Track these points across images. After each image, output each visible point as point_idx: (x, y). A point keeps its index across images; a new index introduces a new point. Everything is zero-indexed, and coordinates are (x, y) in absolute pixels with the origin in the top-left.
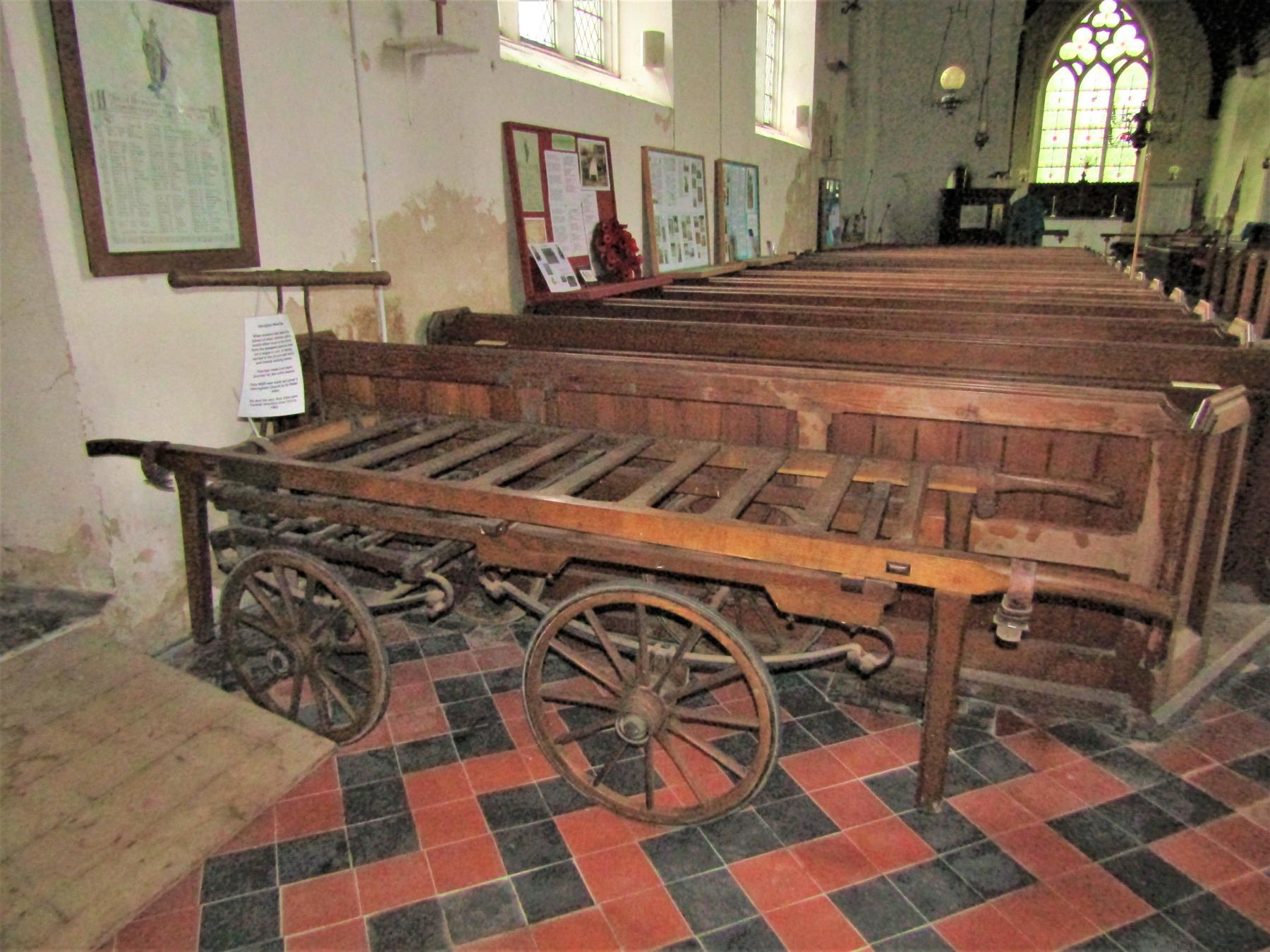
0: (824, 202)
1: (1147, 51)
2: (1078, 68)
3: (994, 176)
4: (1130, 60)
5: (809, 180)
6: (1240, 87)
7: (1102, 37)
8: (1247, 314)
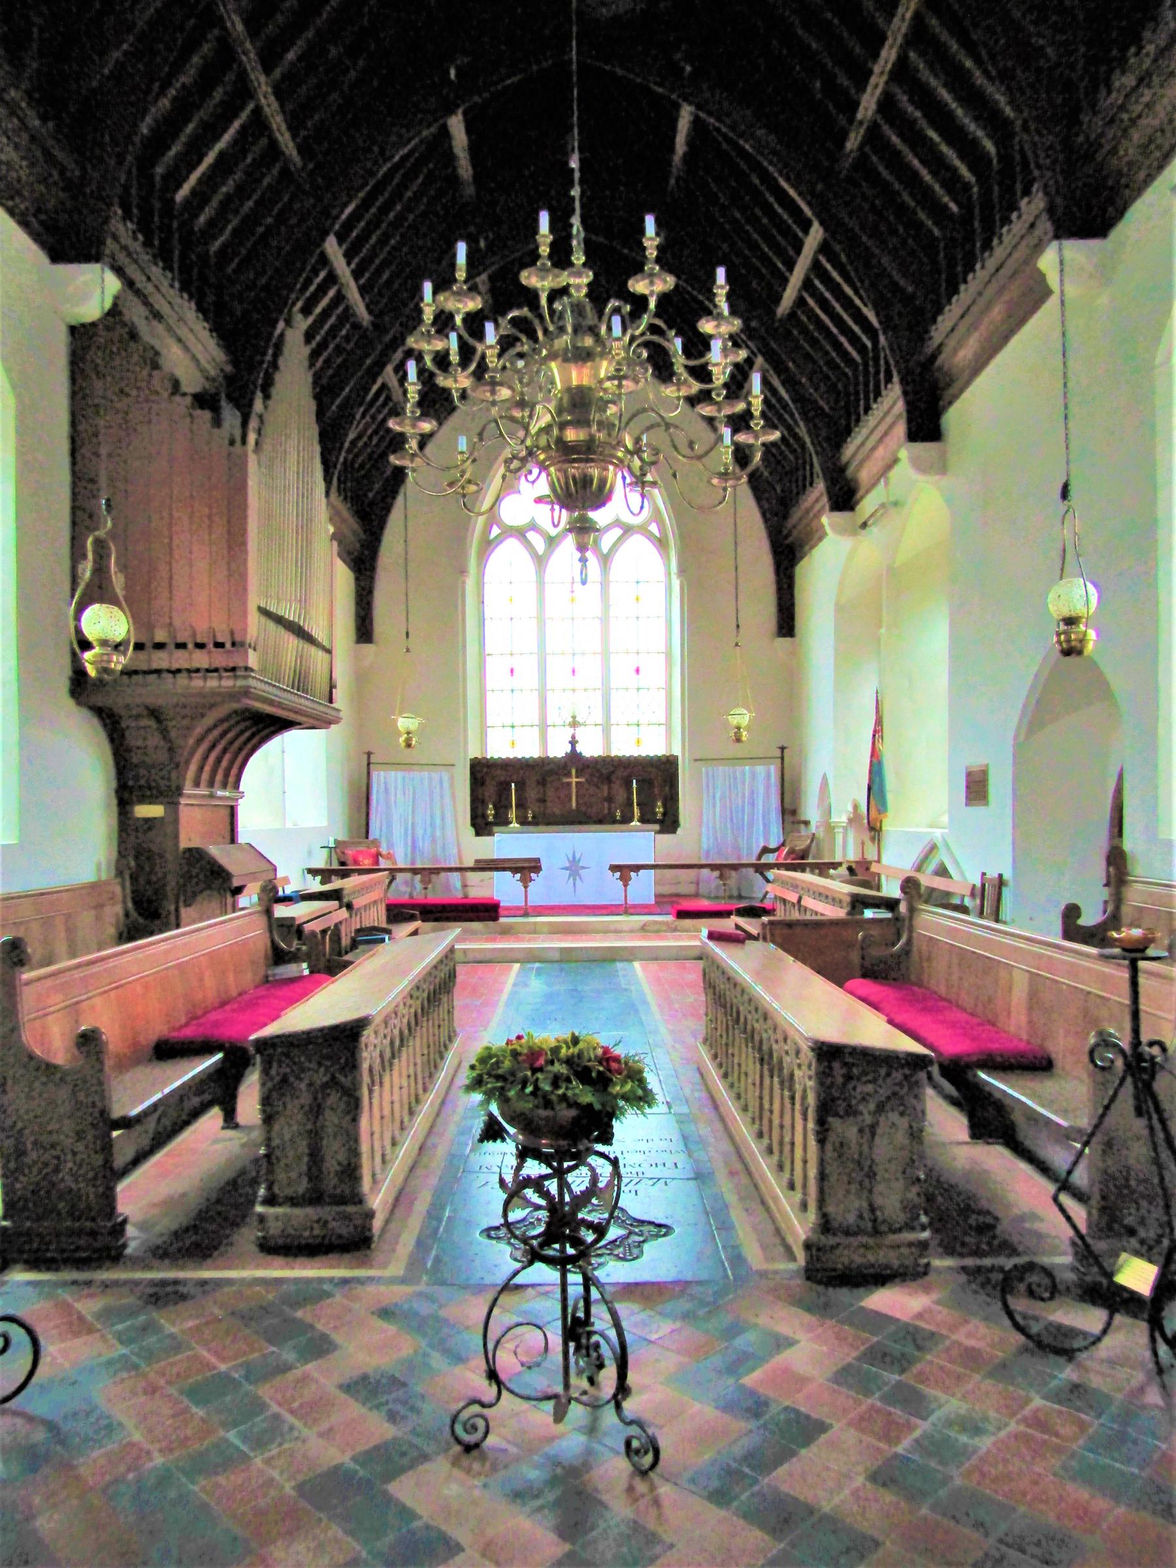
1: (656, 517)
4: (628, 530)
6: (836, 558)
8: (666, 890)
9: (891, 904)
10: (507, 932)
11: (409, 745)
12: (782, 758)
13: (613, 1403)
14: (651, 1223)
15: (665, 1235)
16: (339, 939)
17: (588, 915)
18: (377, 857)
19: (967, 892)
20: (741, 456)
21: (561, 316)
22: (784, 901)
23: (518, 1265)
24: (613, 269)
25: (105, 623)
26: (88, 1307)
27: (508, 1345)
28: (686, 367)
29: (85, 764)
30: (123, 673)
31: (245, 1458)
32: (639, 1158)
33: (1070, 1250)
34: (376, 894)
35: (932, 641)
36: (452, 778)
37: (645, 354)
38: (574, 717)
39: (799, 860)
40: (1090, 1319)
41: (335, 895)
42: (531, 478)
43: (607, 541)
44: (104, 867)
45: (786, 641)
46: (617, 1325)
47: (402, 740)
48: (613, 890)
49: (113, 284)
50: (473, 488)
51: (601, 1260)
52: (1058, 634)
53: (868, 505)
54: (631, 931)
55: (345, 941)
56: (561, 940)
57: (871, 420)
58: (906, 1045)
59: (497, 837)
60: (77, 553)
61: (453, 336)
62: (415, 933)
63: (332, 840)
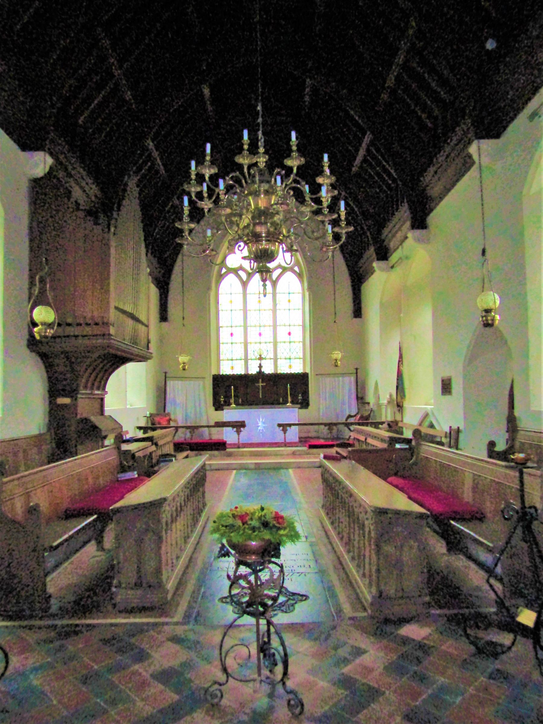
1: (297, 263)
2: (244, 276)
6: (380, 282)
8: (303, 435)
9: (408, 441)
10: (230, 455)
11: (184, 369)
12: (357, 373)
13: (281, 683)
14: (299, 594)
15: (306, 599)
16: (152, 459)
17: (269, 447)
18: (169, 420)
19: (443, 435)
20: (337, 237)
21: (254, 176)
22: (359, 440)
23: (237, 616)
24: (277, 156)
25: (43, 314)
26: (31, 637)
27: (231, 654)
28: (311, 199)
29: (34, 380)
30: (52, 337)
31: (105, 712)
32: (293, 563)
33: (495, 605)
34: (169, 439)
35: (424, 319)
36: (204, 383)
37: (292, 193)
38: (260, 355)
39: (365, 420)
40: (506, 639)
41: (149, 439)
42: (240, 249)
43: (275, 275)
44: (42, 427)
45: (357, 320)
46: (283, 644)
47: (181, 366)
48: (279, 436)
49: (50, 161)
50: (214, 253)
51: (275, 612)
52: (482, 317)
53: (394, 258)
54: (288, 455)
55: (154, 461)
56: (255, 459)
57: (395, 220)
58: (417, 508)
59: (225, 411)
60: (32, 284)
61: (205, 185)
62: (187, 457)
63: (148, 413)
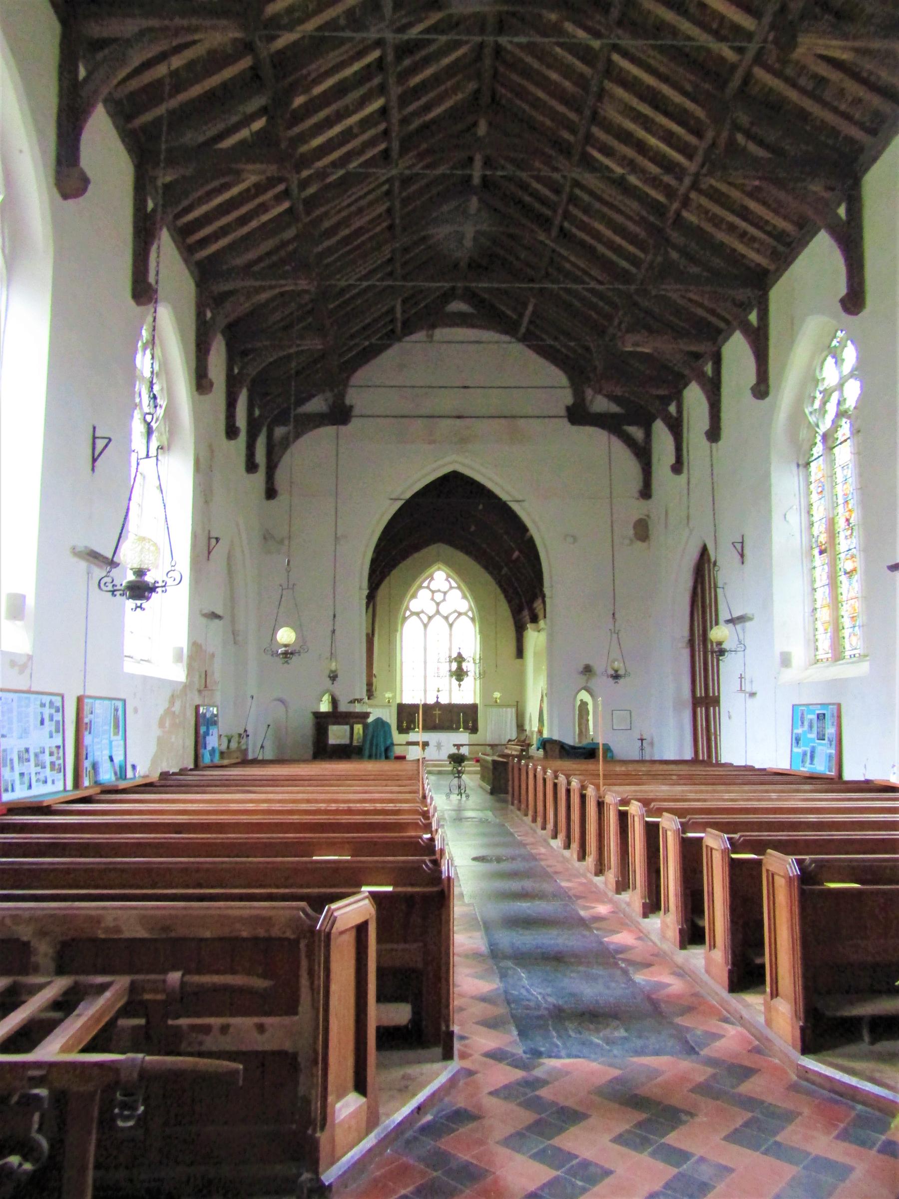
0: (202, 724)
1: (471, 609)
3: (353, 702)
4: (460, 614)
5: (183, 708)
7: (439, 597)
45: (519, 660)
